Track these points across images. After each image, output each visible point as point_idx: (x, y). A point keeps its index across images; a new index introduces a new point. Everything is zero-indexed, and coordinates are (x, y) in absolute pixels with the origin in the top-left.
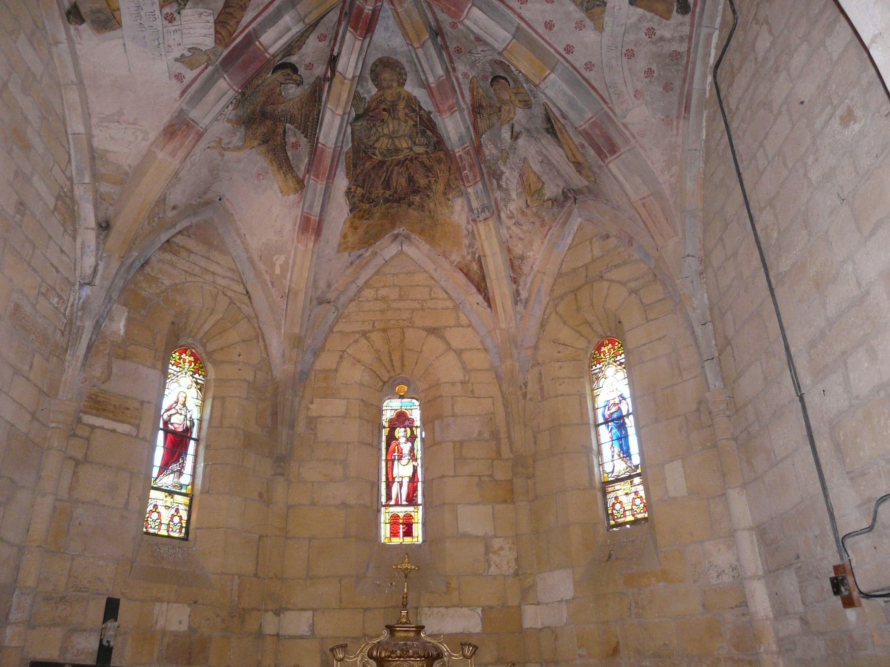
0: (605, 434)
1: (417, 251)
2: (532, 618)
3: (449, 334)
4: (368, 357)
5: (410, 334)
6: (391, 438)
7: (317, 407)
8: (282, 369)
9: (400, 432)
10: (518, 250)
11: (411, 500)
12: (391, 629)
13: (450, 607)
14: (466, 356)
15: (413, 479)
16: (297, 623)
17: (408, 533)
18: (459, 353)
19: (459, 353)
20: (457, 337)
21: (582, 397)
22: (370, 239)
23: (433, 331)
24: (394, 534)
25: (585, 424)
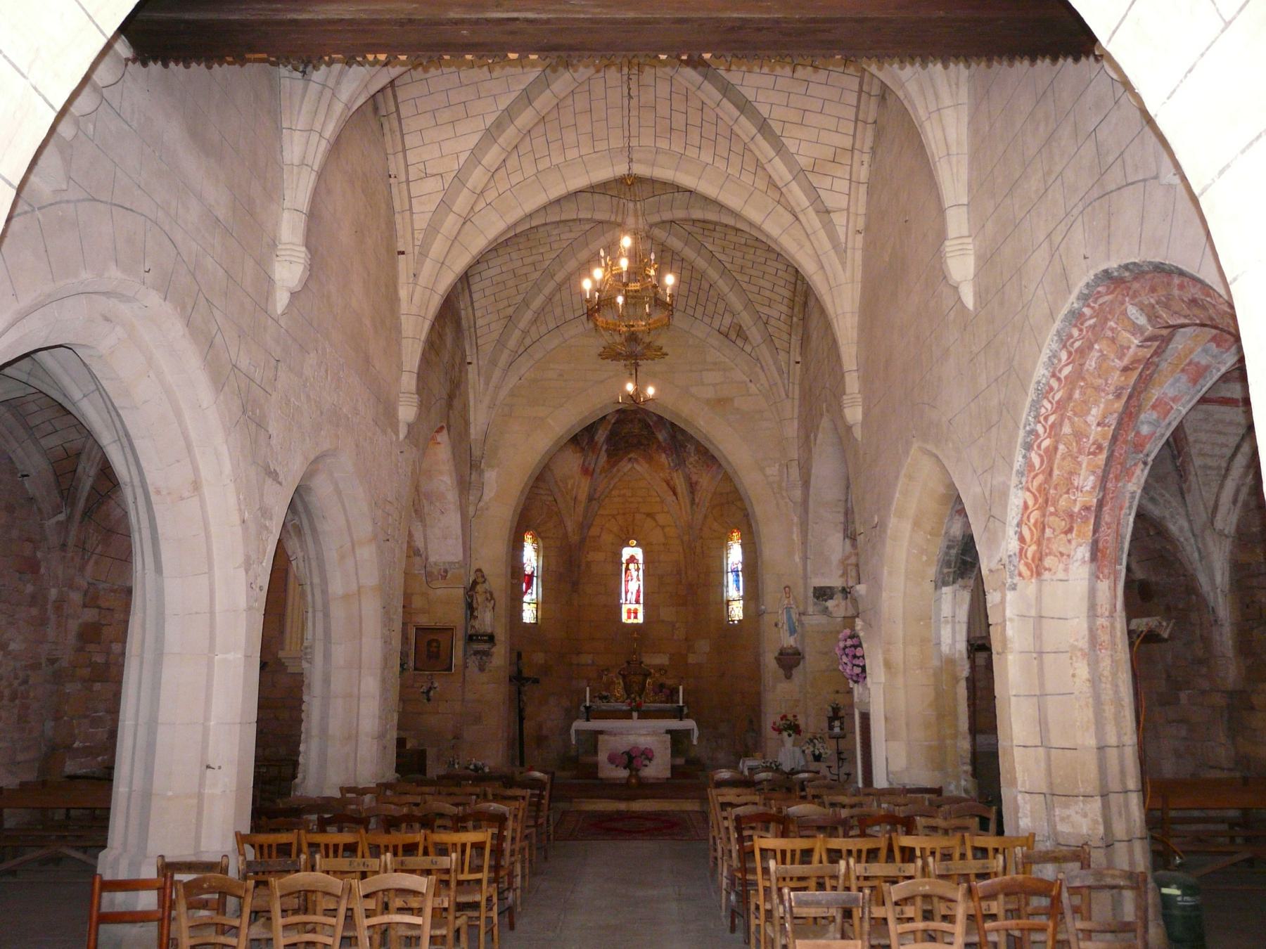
0: (731, 577)
1: (641, 468)
2: (692, 659)
3: (658, 517)
4: (615, 529)
5: (638, 516)
6: (627, 569)
7: (592, 556)
8: (574, 539)
9: (632, 566)
10: (695, 478)
11: (637, 602)
12: (628, 663)
13: (18, 194)
14: (667, 530)
15: (638, 591)
16: (586, 659)
17: (636, 617)
18: (663, 527)
19: (663, 527)
20: (661, 518)
21: (722, 559)
22: (615, 464)
23: (648, 515)
24: (629, 617)
25: (721, 572)
